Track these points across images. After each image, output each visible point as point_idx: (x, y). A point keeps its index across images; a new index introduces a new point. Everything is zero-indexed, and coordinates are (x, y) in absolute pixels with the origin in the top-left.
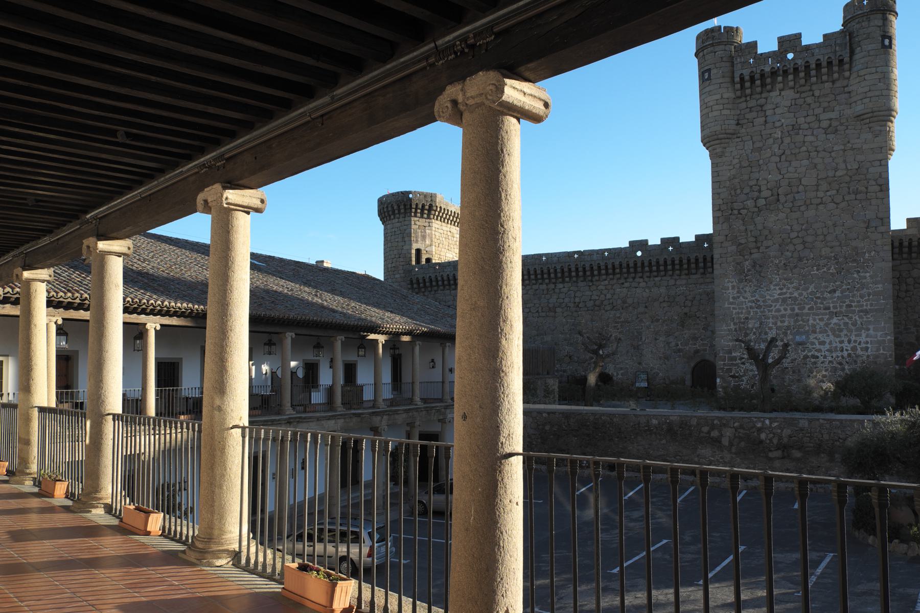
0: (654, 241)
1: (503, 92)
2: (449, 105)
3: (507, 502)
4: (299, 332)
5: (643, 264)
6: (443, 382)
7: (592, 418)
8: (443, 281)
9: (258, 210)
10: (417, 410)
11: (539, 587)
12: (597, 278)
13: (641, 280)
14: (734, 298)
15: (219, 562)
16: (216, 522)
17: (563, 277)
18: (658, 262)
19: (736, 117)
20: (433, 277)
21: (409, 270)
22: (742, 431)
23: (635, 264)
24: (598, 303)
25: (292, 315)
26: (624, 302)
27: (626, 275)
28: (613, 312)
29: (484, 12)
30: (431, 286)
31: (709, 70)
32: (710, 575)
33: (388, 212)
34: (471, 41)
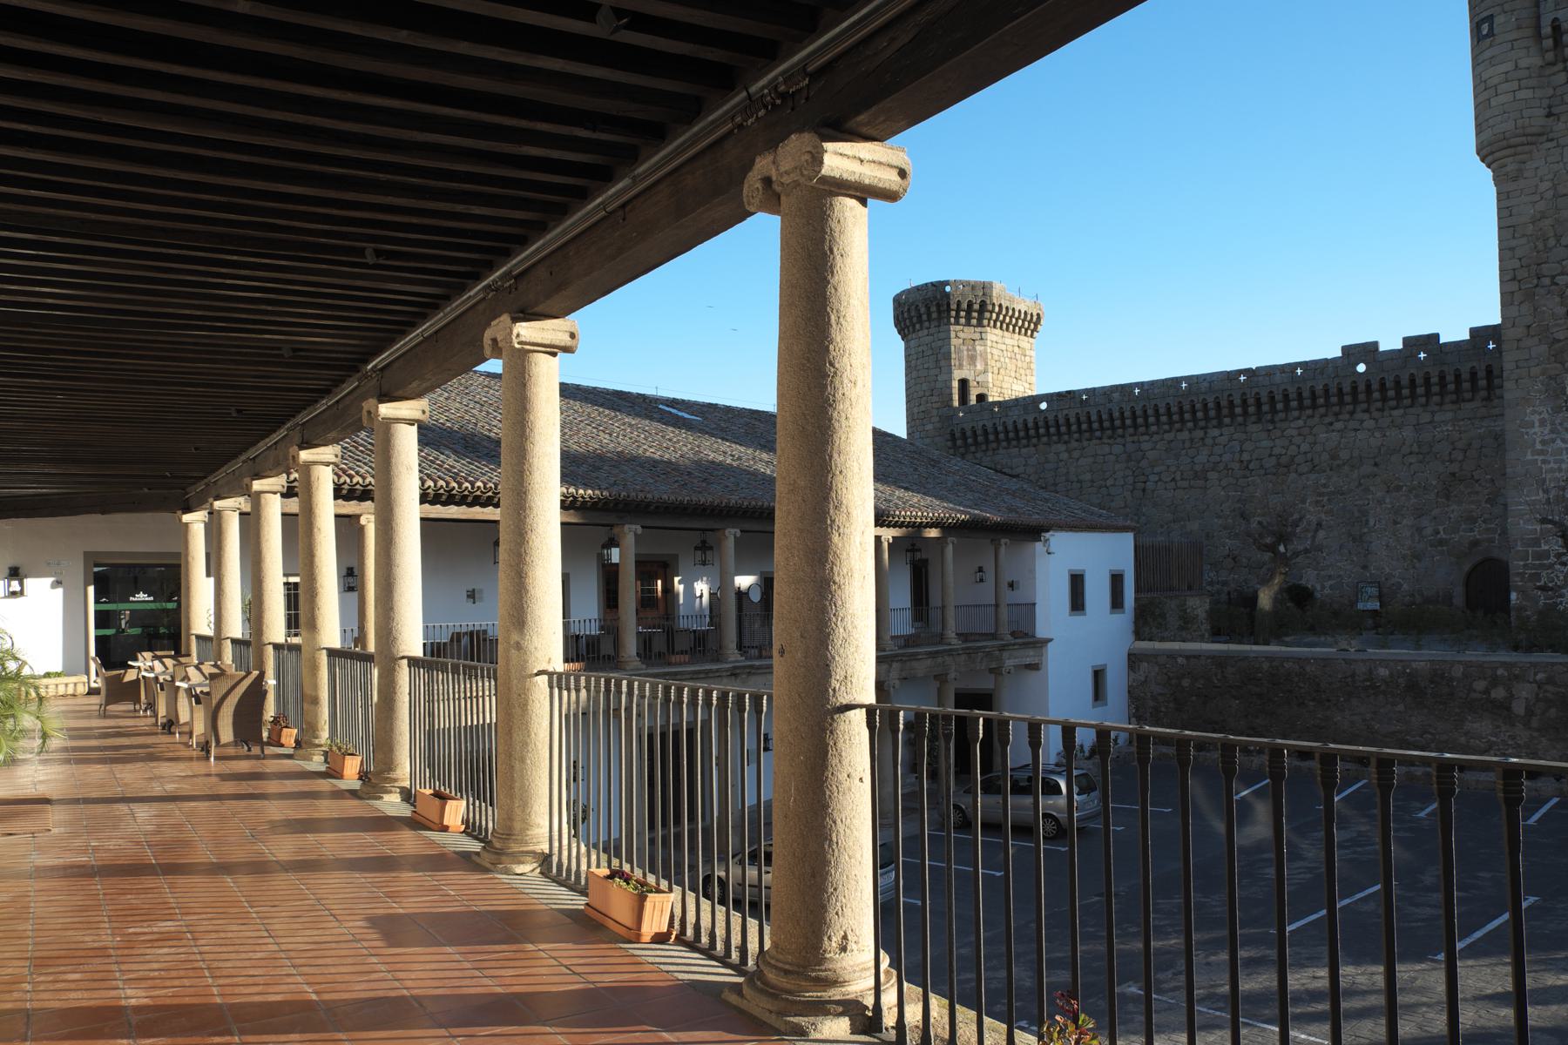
0: (1390, 342)
1: (822, 162)
2: (759, 185)
3: (843, 776)
4: (747, 526)
5: (1368, 386)
6: (997, 606)
7: (1266, 666)
8: (1007, 432)
9: (567, 350)
10: (950, 652)
11: (1158, 951)
12: (1282, 415)
13: (1366, 416)
14: (1543, 442)
15: (520, 869)
16: (518, 811)
17: (1219, 416)
18: (1397, 383)
19: (1546, 102)
20: (989, 425)
21: (948, 415)
22: (1549, 688)
23: (1355, 388)
24: (1284, 460)
25: (734, 499)
26: (1334, 457)
27: (1336, 409)
28: (1313, 476)
29: (800, 42)
30: (987, 442)
31: (1490, 18)
32: (1459, 946)
33: (911, 318)
34: (782, 88)
